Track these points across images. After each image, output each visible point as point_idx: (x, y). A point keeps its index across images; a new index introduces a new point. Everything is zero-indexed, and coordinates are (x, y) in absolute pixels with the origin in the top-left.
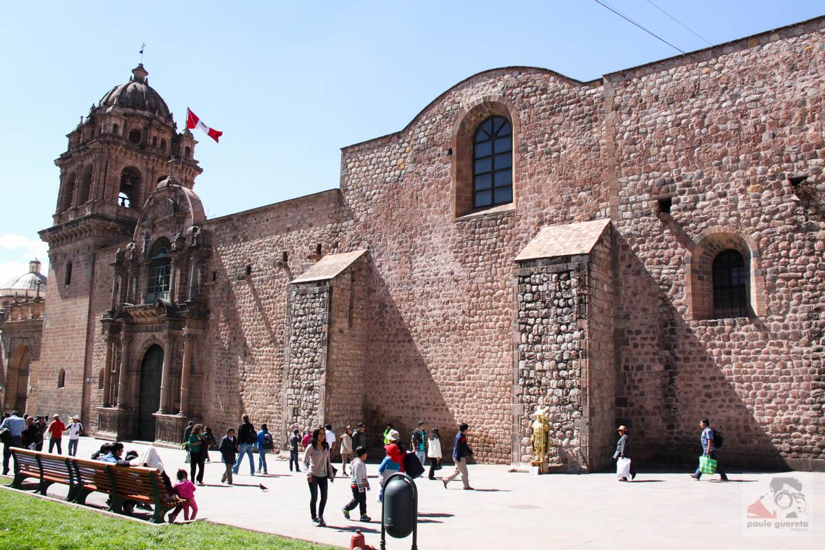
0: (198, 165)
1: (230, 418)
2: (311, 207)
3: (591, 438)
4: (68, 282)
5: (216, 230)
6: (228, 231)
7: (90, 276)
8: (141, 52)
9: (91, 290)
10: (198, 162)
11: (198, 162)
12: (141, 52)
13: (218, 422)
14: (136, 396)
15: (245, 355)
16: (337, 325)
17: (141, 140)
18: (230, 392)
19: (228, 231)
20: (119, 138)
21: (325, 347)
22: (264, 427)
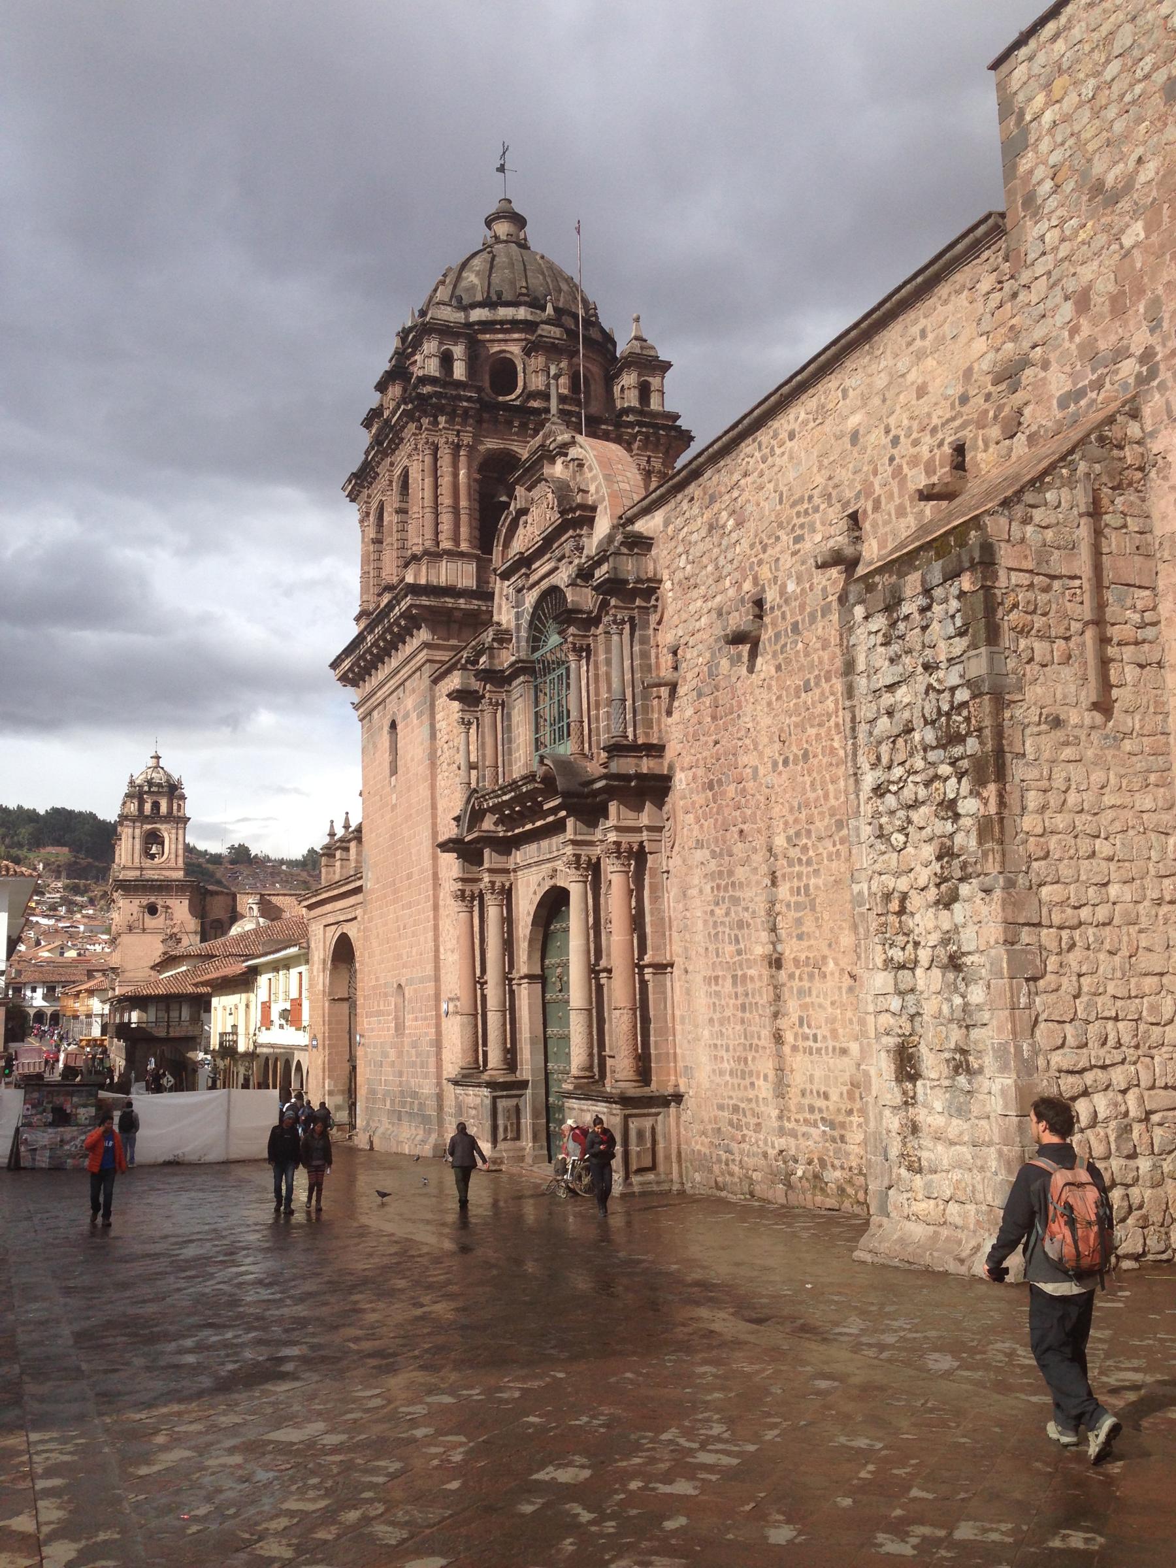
0: (678, 423)
1: (751, 1094)
2: (915, 330)
3: (754, 1211)
4: (394, 771)
5: (667, 523)
6: (696, 510)
7: (427, 743)
8: (502, 169)
9: (433, 776)
10: (677, 417)
11: (677, 417)
12: (502, 169)
13: (721, 1107)
14: (533, 1041)
15: (774, 883)
16: (1034, 693)
17: (520, 384)
18: (743, 1008)
19: (696, 510)
20: (459, 384)
21: (991, 790)
22: (721, 1107)
